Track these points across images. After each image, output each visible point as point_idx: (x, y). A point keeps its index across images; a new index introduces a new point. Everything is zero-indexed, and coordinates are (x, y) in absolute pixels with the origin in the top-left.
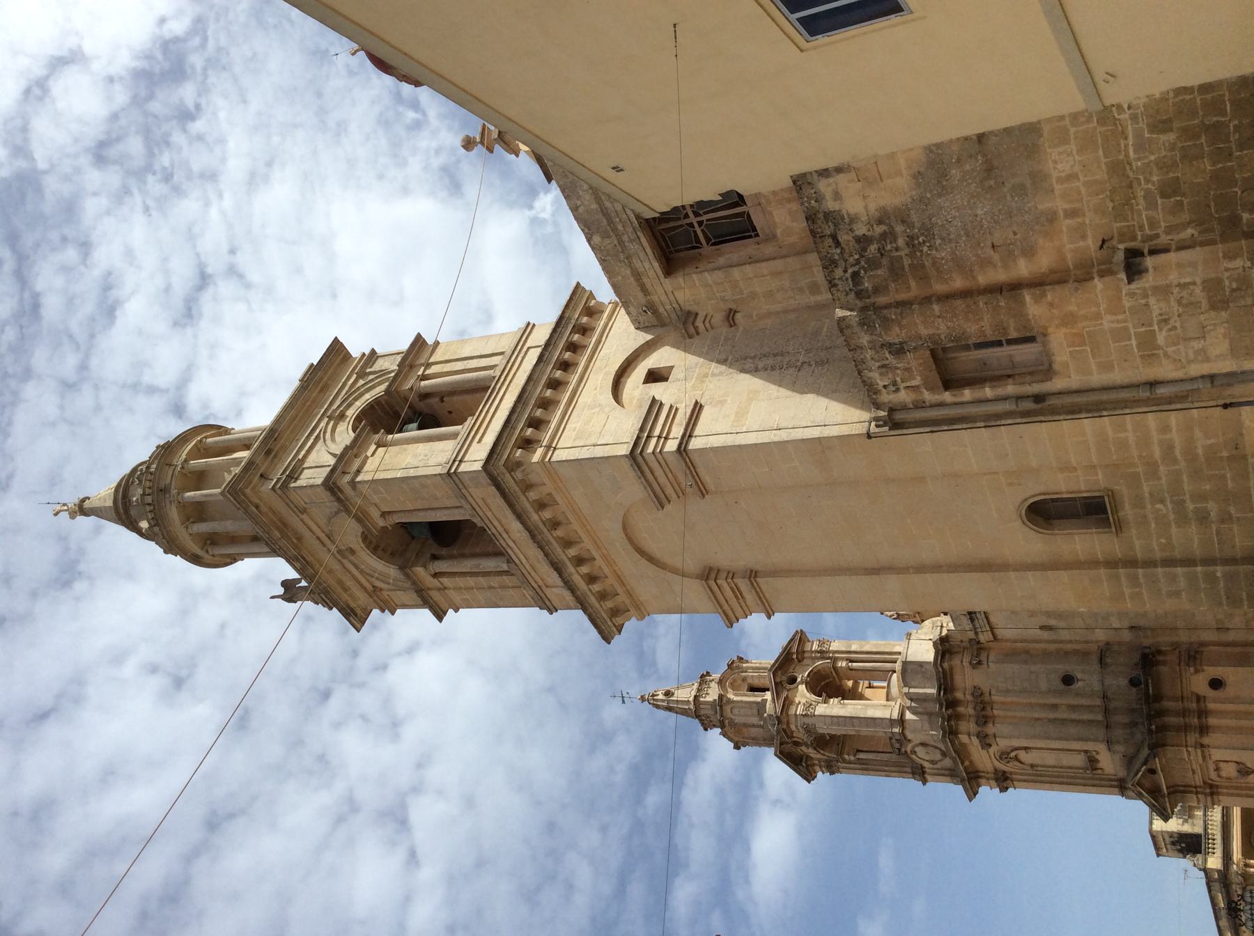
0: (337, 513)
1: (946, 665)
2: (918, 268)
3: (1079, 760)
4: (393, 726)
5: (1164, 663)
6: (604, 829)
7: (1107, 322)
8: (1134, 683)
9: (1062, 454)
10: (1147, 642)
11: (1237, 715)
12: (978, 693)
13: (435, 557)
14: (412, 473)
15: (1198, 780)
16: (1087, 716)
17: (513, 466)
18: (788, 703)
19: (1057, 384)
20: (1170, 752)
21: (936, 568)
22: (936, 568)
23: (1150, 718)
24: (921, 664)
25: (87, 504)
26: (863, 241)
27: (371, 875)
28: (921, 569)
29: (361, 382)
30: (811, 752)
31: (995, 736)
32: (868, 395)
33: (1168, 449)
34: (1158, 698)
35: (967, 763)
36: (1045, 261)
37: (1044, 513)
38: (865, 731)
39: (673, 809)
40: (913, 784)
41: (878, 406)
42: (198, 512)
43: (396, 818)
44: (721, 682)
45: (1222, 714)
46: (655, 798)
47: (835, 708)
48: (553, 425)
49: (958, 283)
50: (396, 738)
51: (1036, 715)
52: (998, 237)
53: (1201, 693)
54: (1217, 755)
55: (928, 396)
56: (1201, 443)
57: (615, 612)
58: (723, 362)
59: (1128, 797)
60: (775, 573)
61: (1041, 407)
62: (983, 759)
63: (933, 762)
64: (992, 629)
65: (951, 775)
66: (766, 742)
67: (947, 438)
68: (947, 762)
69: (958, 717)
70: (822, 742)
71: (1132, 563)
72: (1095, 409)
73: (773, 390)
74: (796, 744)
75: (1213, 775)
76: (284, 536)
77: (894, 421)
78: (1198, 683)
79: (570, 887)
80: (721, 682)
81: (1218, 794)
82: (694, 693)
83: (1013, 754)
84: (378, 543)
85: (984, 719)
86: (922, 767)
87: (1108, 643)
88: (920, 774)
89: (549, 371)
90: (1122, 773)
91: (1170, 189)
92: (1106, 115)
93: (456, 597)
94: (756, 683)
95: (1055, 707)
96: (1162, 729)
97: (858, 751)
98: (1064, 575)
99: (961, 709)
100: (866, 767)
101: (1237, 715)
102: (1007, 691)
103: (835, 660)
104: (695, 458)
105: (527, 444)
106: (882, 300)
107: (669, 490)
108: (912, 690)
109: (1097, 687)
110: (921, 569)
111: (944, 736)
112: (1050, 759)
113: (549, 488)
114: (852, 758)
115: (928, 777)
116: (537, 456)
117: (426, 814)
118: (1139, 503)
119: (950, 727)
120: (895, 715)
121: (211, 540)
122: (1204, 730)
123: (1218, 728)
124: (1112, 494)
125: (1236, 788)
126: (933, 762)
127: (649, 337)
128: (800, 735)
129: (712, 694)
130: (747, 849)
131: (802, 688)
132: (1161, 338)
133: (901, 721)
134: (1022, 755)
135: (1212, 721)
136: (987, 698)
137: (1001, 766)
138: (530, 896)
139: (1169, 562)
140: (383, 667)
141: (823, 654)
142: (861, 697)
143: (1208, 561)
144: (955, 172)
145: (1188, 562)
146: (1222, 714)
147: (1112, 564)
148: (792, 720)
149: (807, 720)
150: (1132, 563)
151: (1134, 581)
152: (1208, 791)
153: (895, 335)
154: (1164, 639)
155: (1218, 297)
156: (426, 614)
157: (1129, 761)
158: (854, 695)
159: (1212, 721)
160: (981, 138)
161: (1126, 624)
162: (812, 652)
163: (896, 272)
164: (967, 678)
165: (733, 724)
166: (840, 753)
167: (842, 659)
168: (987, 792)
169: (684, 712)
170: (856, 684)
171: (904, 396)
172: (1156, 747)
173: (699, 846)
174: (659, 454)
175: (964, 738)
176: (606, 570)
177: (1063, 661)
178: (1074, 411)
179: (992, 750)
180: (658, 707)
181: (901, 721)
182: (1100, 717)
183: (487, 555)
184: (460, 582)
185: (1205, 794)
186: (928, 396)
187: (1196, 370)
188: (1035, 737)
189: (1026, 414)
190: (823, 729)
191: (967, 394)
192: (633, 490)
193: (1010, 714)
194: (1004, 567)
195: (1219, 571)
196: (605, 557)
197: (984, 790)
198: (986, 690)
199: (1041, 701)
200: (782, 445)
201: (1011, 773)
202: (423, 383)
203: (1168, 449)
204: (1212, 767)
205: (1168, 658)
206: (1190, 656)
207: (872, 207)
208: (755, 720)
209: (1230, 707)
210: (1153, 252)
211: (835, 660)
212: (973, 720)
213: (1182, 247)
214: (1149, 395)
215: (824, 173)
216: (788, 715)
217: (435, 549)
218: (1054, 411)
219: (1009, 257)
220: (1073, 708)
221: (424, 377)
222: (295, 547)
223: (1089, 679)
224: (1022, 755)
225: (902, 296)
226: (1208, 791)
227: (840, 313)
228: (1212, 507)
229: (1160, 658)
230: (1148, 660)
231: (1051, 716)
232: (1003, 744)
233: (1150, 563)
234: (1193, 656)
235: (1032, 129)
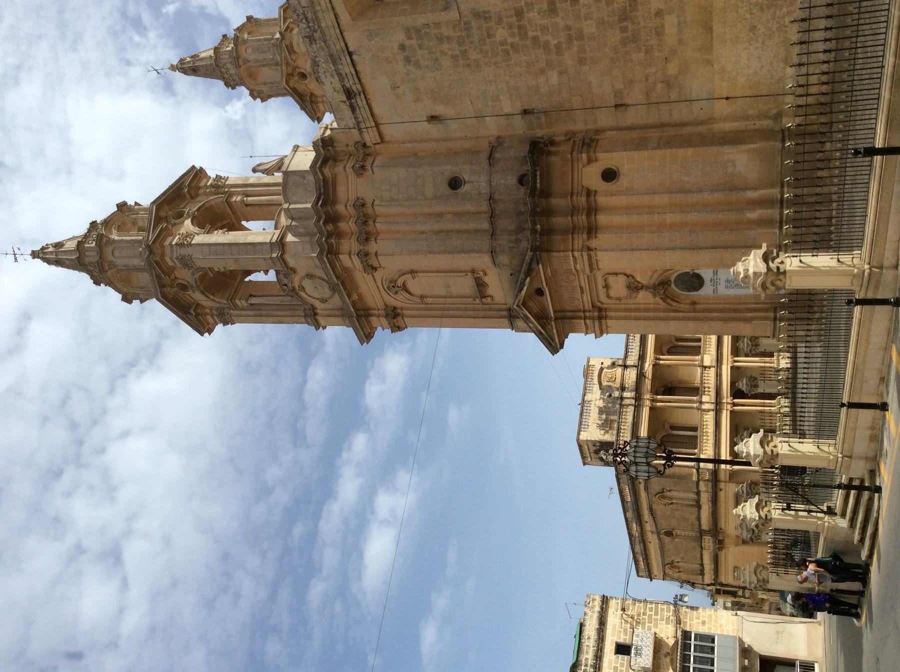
1: (327, 171)
3: (465, 286)
4: (109, 490)
5: (556, 153)
6: (264, 554)
8: (521, 180)
10: (539, 133)
11: (629, 209)
12: (360, 204)
16: (472, 225)
27: (93, 600)
30: (198, 296)
31: (376, 254)
34: (546, 193)
35: (355, 297)
39: (312, 537)
43: (113, 556)
46: (298, 530)
50: (113, 500)
51: (420, 227)
53: (593, 188)
59: (519, 330)
63: (324, 301)
64: (377, 125)
69: (340, 235)
75: (602, 292)
78: (591, 176)
79: (237, 596)
81: (606, 317)
83: (400, 282)
85: (366, 237)
86: (314, 308)
87: (498, 137)
95: (440, 215)
96: (549, 232)
97: (251, 296)
99: (343, 225)
101: (629, 209)
108: (292, 206)
109: (484, 188)
111: (321, 253)
114: (245, 304)
115: (320, 319)
117: (135, 552)
119: (330, 246)
122: (592, 230)
123: (609, 228)
125: (627, 310)
126: (324, 301)
128: (184, 275)
130: (361, 556)
136: (369, 210)
138: (209, 604)
140: (102, 451)
142: (244, 229)
148: (168, 252)
149: (184, 251)
152: (596, 314)
154: (558, 130)
161: (518, 107)
162: (206, 186)
164: (350, 187)
167: (238, 193)
173: (330, 558)
179: (378, 275)
181: (281, 243)
182: (485, 225)
185: (593, 318)
193: (394, 228)
198: (369, 201)
199: (428, 210)
201: (402, 309)
204: (600, 283)
205: (562, 148)
206: (584, 144)
212: (354, 237)
216: (163, 247)
223: (477, 181)
226: (596, 314)
229: (553, 149)
230: (538, 149)
231: (436, 227)
234: (588, 143)
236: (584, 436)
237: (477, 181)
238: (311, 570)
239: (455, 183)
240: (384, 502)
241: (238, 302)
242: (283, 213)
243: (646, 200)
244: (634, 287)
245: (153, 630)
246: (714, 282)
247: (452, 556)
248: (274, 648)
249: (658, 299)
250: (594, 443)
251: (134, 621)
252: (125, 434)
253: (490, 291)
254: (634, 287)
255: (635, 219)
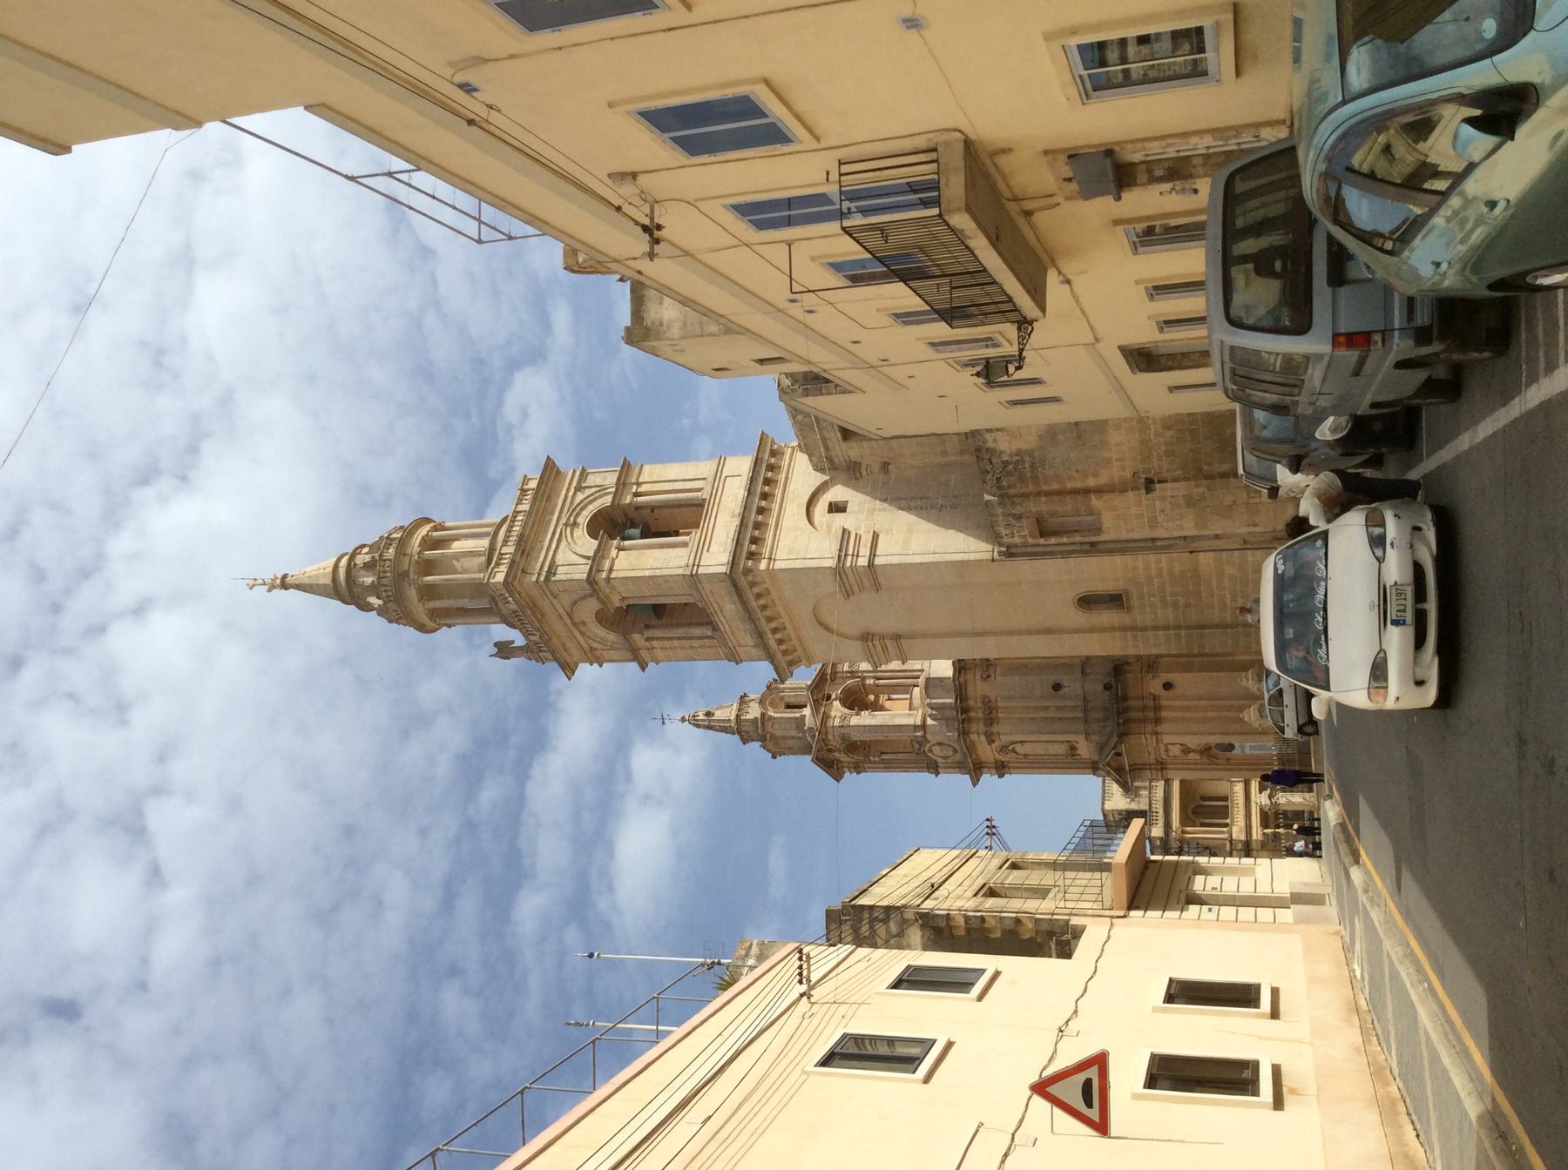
0: (584, 598)
2: (1035, 478)
3: (1061, 749)
6: (423, 832)
7: (1134, 510)
8: (1107, 687)
9: (1101, 573)
11: (1182, 709)
13: (647, 626)
14: (658, 573)
15: (1152, 759)
17: (747, 571)
18: (826, 717)
19: (1103, 538)
20: (1133, 739)
21: (1020, 632)
22: (1020, 632)
23: (1119, 713)
24: (941, 680)
25: (289, 580)
26: (1006, 463)
28: (1011, 633)
29: (580, 496)
30: (843, 757)
32: (995, 538)
33: (1160, 571)
34: (1125, 698)
36: (1103, 479)
37: (1087, 602)
38: (892, 736)
40: (926, 777)
41: (1000, 545)
42: (429, 592)
43: (128, 826)
44: (761, 702)
45: (1171, 708)
46: (490, 794)
47: (866, 719)
48: (769, 542)
49: (1055, 486)
50: (124, 722)
52: (1080, 467)
54: (1167, 739)
55: (1030, 540)
56: (1177, 568)
57: (792, 664)
58: (885, 500)
60: (913, 636)
61: (1093, 548)
62: (987, 752)
65: (960, 767)
66: (806, 750)
67: (1039, 563)
68: (958, 757)
69: (970, 720)
70: (852, 747)
71: (1134, 628)
72: (1123, 551)
73: (924, 525)
74: (830, 750)
76: (534, 613)
77: (1010, 553)
78: (1155, 686)
80: (761, 702)
82: (734, 714)
84: (602, 618)
85: (990, 721)
88: (934, 768)
89: (757, 502)
90: (1095, 757)
91: (1170, 454)
92: (1141, 420)
93: (660, 654)
94: (793, 701)
95: (1046, 708)
98: (1096, 635)
99: (972, 714)
100: (889, 766)
101: (1182, 709)
102: (1009, 698)
103: (864, 678)
104: (878, 570)
105: (752, 555)
106: (1012, 491)
107: (855, 587)
109: (1078, 689)
110: (1011, 633)
112: (1039, 749)
113: (768, 584)
116: (763, 565)
117: (169, 822)
118: (1141, 597)
120: (919, 722)
121: (435, 614)
122: (1158, 721)
124: (1126, 592)
127: (826, 478)
128: (834, 741)
129: (754, 712)
131: (837, 704)
132: (1160, 519)
133: (924, 726)
134: (1018, 748)
135: (1164, 714)
137: (1000, 757)
139: (1156, 628)
141: (853, 674)
142: (882, 708)
143: (1178, 627)
144: (1060, 437)
145: (1167, 628)
146: (1171, 708)
147: (1123, 629)
148: (830, 731)
150: (1134, 628)
151: (1135, 638)
153: (1018, 510)
155: (1190, 502)
156: (634, 666)
157: (1101, 748)
158: (876, 707)
159: (1164, 714)
160: (1077, 424)
163: (1022, 478)
164: (978, 689)
165: (774, 737)
166: (867, 756)
168: (987, 779)
169: (724, 730)
170: (877, 697)
171: (1017, 540)
172: (1122, 735)
173: (549, 851)
174: (854, 568)
175: (974, 737)
176: (793, 636)
177: (1054, 676)
178: (1111, 552)
180: (698, 726)
181: (924, 726)
183: (699, 624)
184: (667, 643)
186: (1030, 540)
187: (1176, 534)
188: (1031, 733)
189: (1086, 552)
190: (856, 737)
191: (1053, 540)
192: (830, 586)
194: (1060, 631)
195: (1183, 633)
196: (796, 629)
200: (937, 564)
202: (640, 499)
203: (1160, 571)
204: (1162, 748)
207: (1014, 448)
208: (794, 733)
209: (1177, 703)
210: (1160, 482)
211: (864, 678)
213: (1175, 480)
214: (1152, 545)
215: (990, 431)
217: (654, 622)
218: (1100, 551)
219: (1085, 476)
220: (1059, 708)
221: (636, 495)
222: (540, 621)
223: (1072, 685)
224: (1018, 748)
225: (1024, 490)
227: (987, 497)
228: (1181, 600)
232: (1005, 739)
233: (1145, 629)
234: (1151, 664)
235: (1105, 422)
236: (1109, 806)
237: (1072, 685)
238: (514, 871)
239: (1057, 687)
240: (646, 761)
242: (883, 668)
243: (1195, 703)
245: (215, 963)
247: (777, 863)
248: (455, 1006)
250: (1120, 812)
251: (177, 946)
252: (140, 610)
254: (1186, 750)
255: (1187, 714)
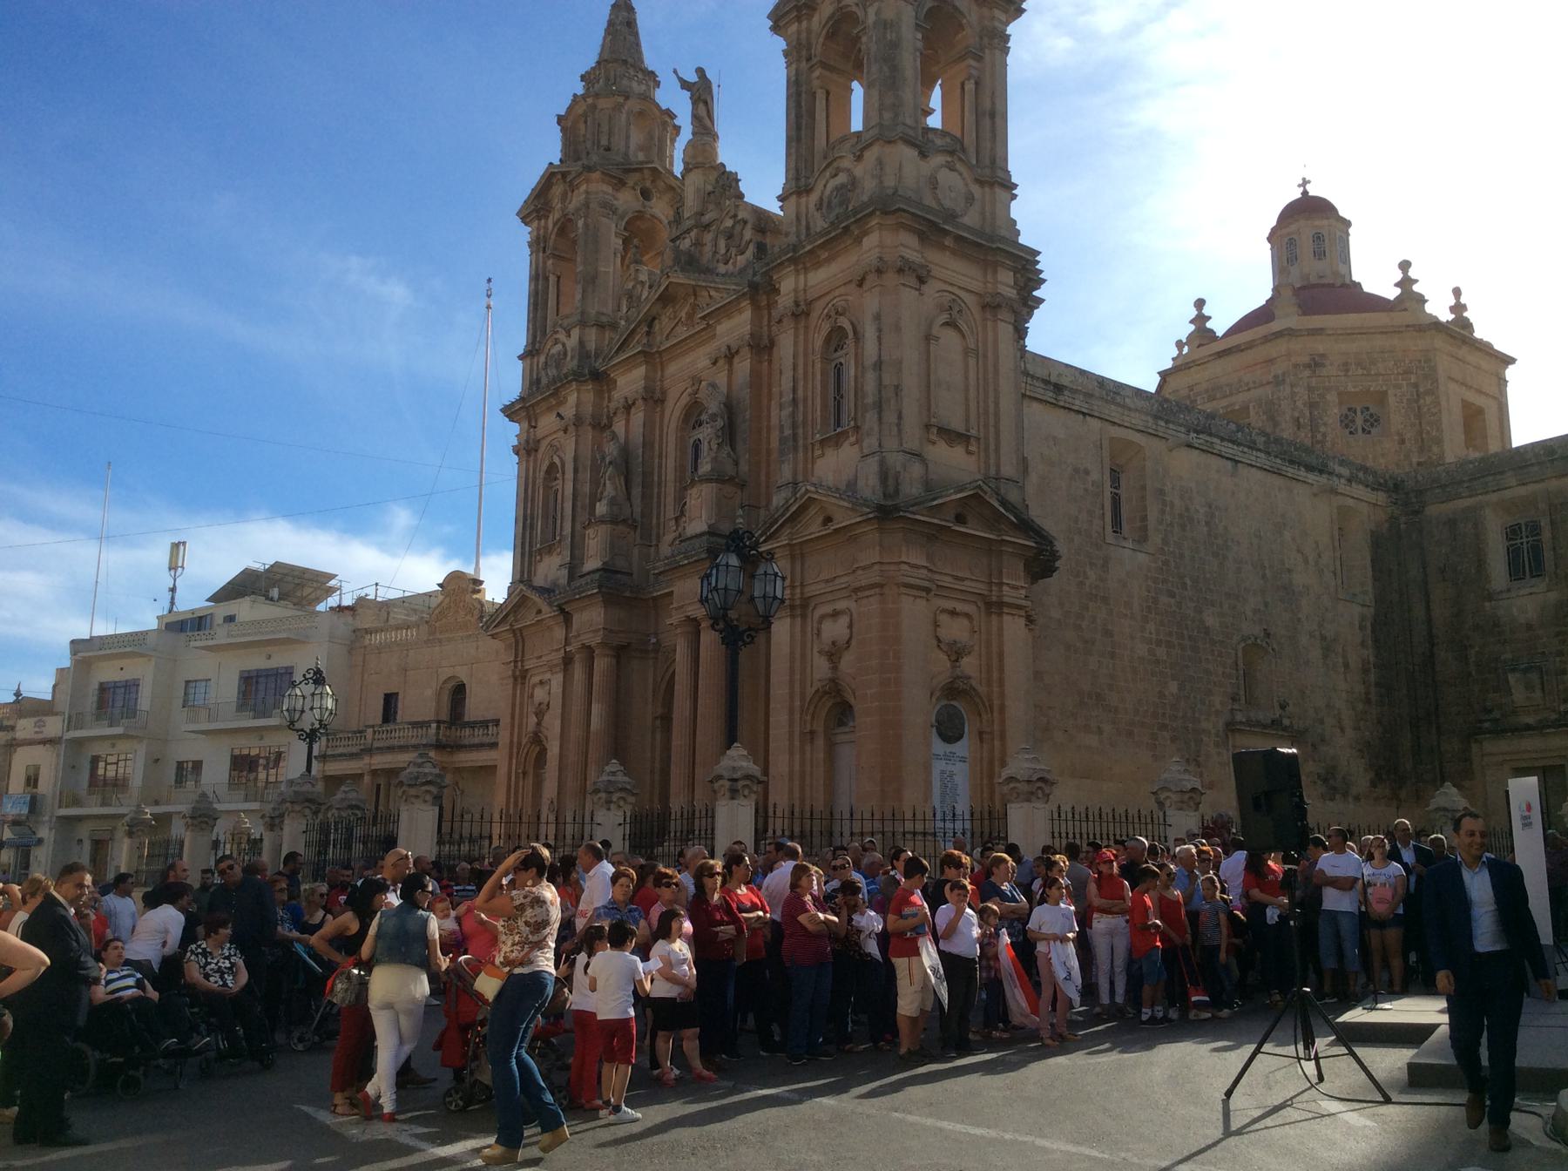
35: (948, 242)
75: (827, 609)
81: (793, 616)
86: (808, 191)
97: (828, 93)
197: (515, 428)
241: (817, 73)
244: (834, 654)
246: (948, 757)
249: (817, 685)
253: (830, 452)
